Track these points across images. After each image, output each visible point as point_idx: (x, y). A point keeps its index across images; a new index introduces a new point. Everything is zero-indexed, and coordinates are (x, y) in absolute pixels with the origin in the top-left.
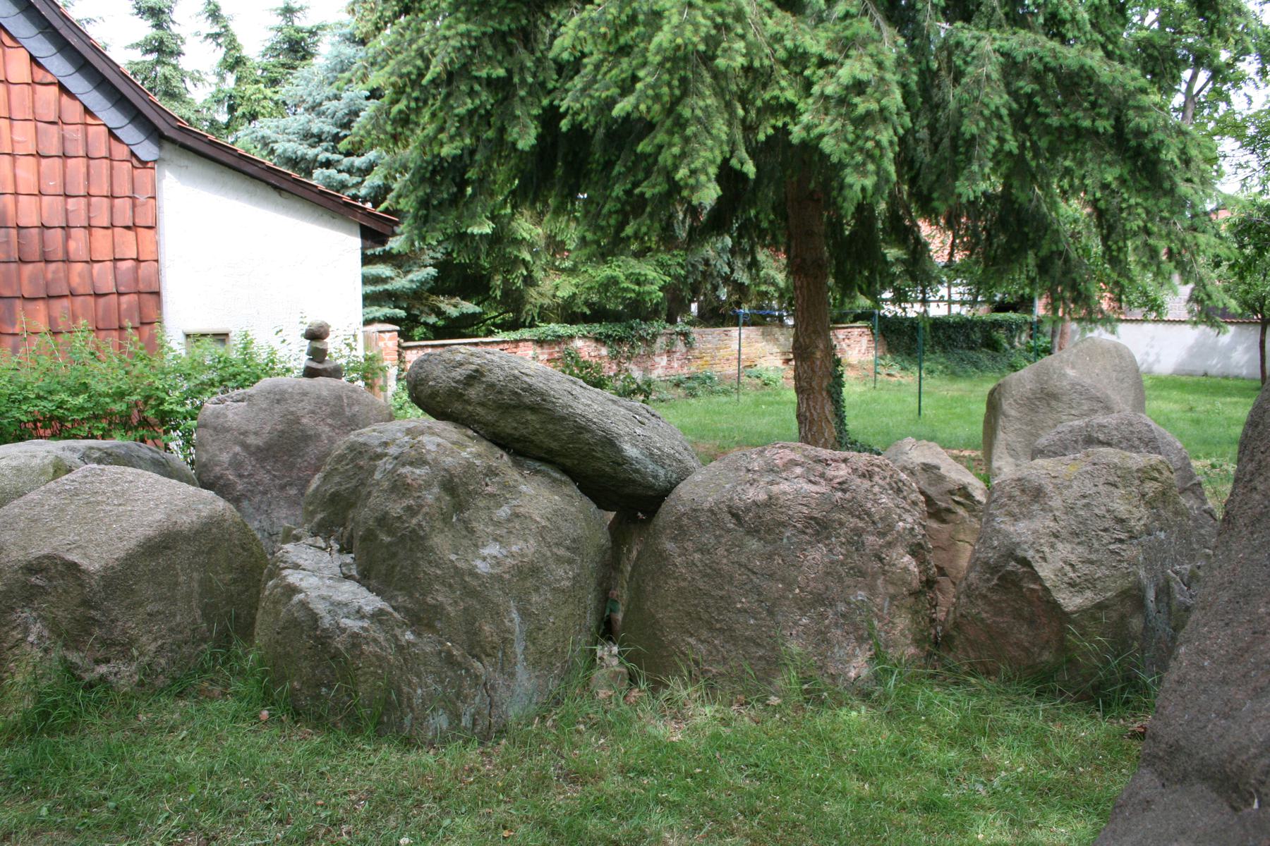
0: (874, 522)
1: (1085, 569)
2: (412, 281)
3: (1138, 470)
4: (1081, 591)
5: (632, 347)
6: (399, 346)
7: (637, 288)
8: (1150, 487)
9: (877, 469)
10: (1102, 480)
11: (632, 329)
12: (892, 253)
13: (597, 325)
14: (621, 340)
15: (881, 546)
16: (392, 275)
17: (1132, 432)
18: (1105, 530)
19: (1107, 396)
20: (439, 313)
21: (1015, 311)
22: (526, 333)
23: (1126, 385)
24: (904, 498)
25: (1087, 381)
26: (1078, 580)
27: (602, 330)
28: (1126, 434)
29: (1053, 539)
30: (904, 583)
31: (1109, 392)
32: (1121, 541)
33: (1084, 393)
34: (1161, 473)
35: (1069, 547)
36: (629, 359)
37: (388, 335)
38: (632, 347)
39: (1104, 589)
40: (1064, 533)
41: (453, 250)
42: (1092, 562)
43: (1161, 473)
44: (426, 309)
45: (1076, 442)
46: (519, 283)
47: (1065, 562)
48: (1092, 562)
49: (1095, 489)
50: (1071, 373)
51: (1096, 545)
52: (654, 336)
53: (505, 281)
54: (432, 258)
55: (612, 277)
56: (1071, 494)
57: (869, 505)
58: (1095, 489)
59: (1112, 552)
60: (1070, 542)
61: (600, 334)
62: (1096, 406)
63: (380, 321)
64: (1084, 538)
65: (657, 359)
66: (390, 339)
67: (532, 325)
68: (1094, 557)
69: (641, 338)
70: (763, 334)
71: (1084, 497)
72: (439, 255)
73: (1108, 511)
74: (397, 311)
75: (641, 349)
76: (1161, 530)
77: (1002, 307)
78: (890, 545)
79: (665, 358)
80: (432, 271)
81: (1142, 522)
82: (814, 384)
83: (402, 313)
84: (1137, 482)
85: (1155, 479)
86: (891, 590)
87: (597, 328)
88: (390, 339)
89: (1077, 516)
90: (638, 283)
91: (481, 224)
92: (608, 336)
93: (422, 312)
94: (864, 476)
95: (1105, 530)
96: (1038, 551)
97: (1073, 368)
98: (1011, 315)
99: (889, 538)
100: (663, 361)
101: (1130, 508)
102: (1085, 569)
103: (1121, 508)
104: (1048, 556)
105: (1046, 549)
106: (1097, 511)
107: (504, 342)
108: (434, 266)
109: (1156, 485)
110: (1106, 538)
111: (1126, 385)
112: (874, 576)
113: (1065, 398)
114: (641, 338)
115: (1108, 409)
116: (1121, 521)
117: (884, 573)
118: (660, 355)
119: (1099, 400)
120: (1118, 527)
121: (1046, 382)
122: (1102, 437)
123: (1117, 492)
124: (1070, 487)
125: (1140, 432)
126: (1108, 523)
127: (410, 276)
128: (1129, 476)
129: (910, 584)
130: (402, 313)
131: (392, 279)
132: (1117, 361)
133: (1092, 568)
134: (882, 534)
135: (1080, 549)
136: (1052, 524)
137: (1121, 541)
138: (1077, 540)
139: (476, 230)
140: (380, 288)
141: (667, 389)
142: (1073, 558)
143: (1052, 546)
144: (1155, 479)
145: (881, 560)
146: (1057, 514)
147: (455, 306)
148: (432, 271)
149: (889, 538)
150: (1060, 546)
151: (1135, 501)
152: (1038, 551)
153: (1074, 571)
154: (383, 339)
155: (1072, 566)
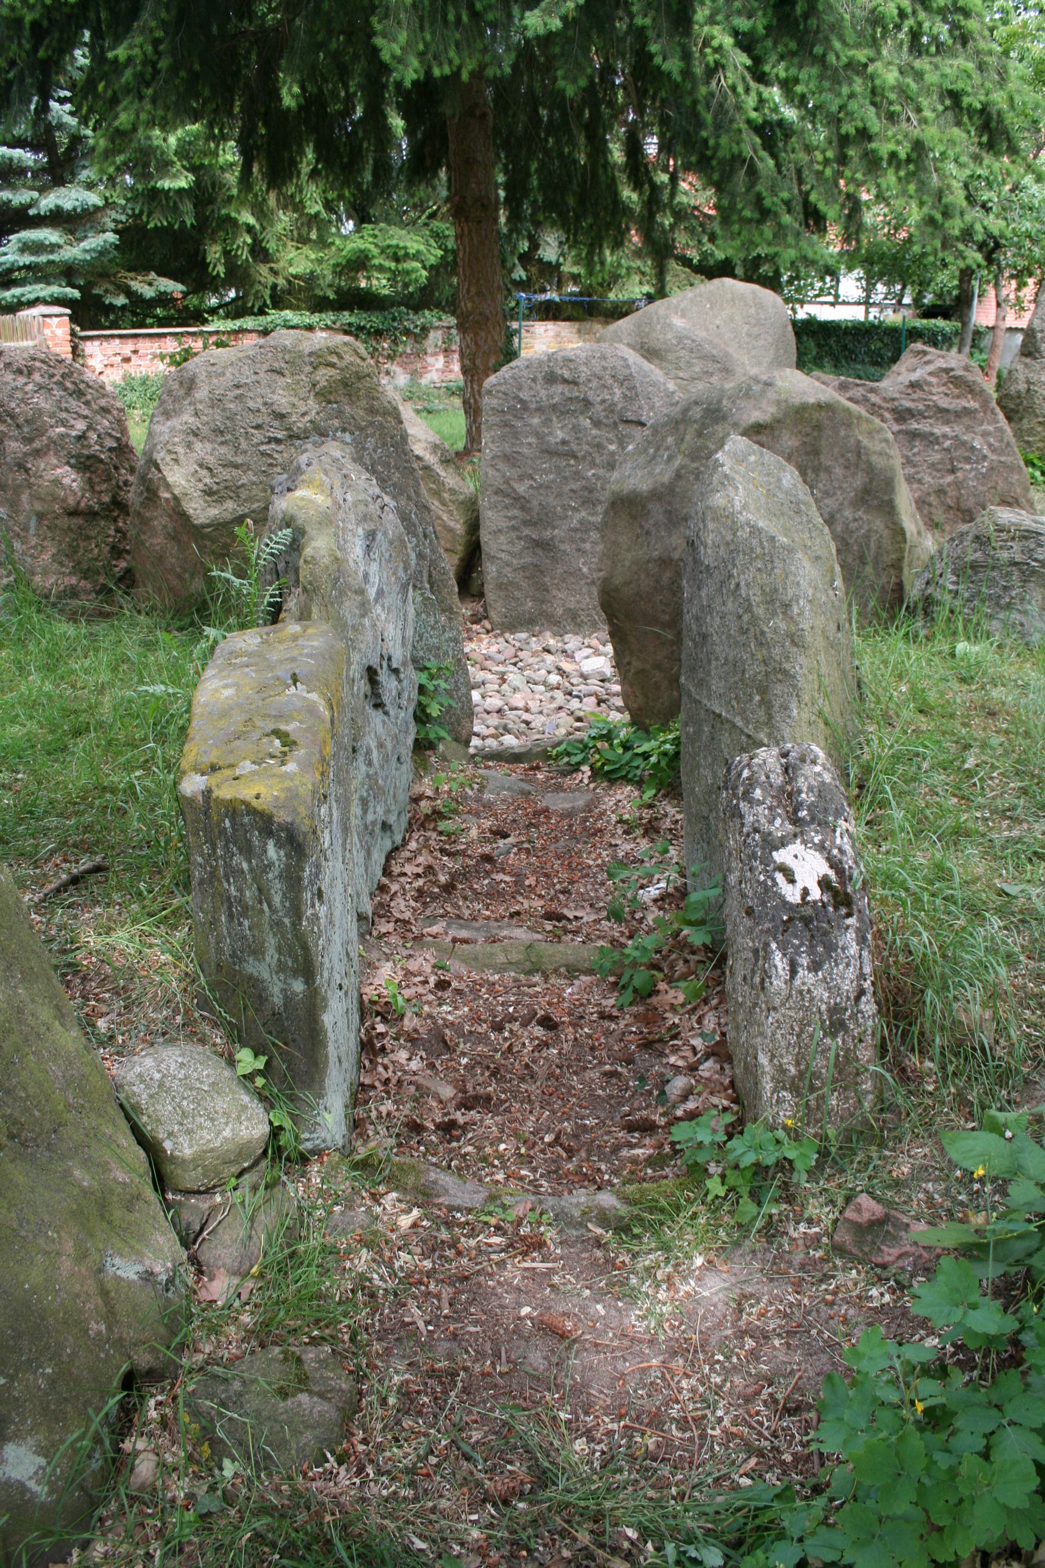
0: (18, 426)
1: (226, 474)
2: (86, 251)
3: (311, 354)
4: (221, 500)
5: (395, 342)
6: (73, 334)
7: (393, 265)
8: (323, 376)
9: (38, 364)
10: (266, 367)
11: (394, 319)
12: (629, 195)
13: (346, 313)
14: (378, 333)
15: (26, 454)
16: (61, 242)
17: (605, 368)
18: (258, 427)
19: (727, 355)
20: (129, 293)
21: (946, 316)
22: (249, 322)
23: (761, 342)
24: (87, 403)
25: (701, 334)
26: (215, 488)
27: (353, 320)
28: (597, 370)
29: (191, 438)
30: (55, 499)
31: (730, 350)
32: (278, 441)
33: (697, 351)
34: (340, 357)
35: (209, 446)
36: (389, 357)
37: (56, 320)
38: (395, 342)
39: (250, 499)
40: (205, 430)
41: (141, 212)
42: (236, 466)
43: (340, 357)
44: (111, 288)
45: (534, 380)
46: (245, 254)
47: (201, 466)
48: (236, 466)
49: (254, 378)
50: (678, 322)
51: (244, 445)
52: (425, 330)
53: (226, 253)
54: (115, 221)
55: (362, 251)
56: (221, 384)
57: (13, 405)
58: (254, 378)
59: (263, 454)
60: (212, 442)
61: (350, 325)
62: (711, 367)
63: (46, 302)
64: (229, 437)
65: (430, 360)
66: (59, 326)
67: (262, 312)
68: (239, 460)
69: (407, 332)
70: (579, 331)
71: (237, 387)
72: (123, 218)
73: (265, 404)
74: (68, 290)
75: (407, 346)
76: (344, 430)
77: (930, 313)
78: (37, 453)
79: (441, 359)
80: (111, 237)
81: (307, 418)
82: (478, 362)
83: (76, 294)
84: (309, 369)
85: (332, 365)
86: (38, 507)
87: (346, 317)
88: (59, 326)
89: (224, 410)
90: (397, 260)
91: (175, 176)
92: (361, 329)
93: (106, 291)
94: (20, 372)
95: (258, 427)
96: (169, 452)
97: (683, 316)
98: (940, 323)
99: (37, 444)
100: (440, 362)
101: (295, 401)
102: (226, 474)
103: (282, 400)
104: (182, 457)
105: (180, 450)
106: (251, 404)
107: (217, 332)
108: (116, 232)
109: (332, 372)
110: (258, 436)
111: (761, 342)
112: (17, 490)
113: (670, 357)
114: (407, 332)
115: (727, 371)
116: (282, 416)
117: (30, 486)
118: (435, 354)
119: (714, 360)
120: (276, 423)
121: (647, 335)
122: (567, 374)
123: (281, 381)
124: (223, 374)
125: (614, 368)
126: (263, 418)
127: (85, 244)
128: (298, 361)
129: (64, 500)
130: (76, 294)
131: (60, 247)
132: (752, 311)
133: (235, 472)
134: (29, 440)
135: (223, 450)
136: (191, 420)
137: (278, 441)
138: (220, 439)
139: (166, 184)
140: (43, 259)
141: (439, 397)
142: (211, 460)
143: (189, 446)
144: (332, 365)
145: (27, 470)
146: (200, 407)
147: (150, 284)
148: (111, 237)
149: (37, 444)
150: (198, 446)
151: (303, 392)
152: (169, 452)
153: (212, 476)
154: (50, 326)
155: (210, 469)
